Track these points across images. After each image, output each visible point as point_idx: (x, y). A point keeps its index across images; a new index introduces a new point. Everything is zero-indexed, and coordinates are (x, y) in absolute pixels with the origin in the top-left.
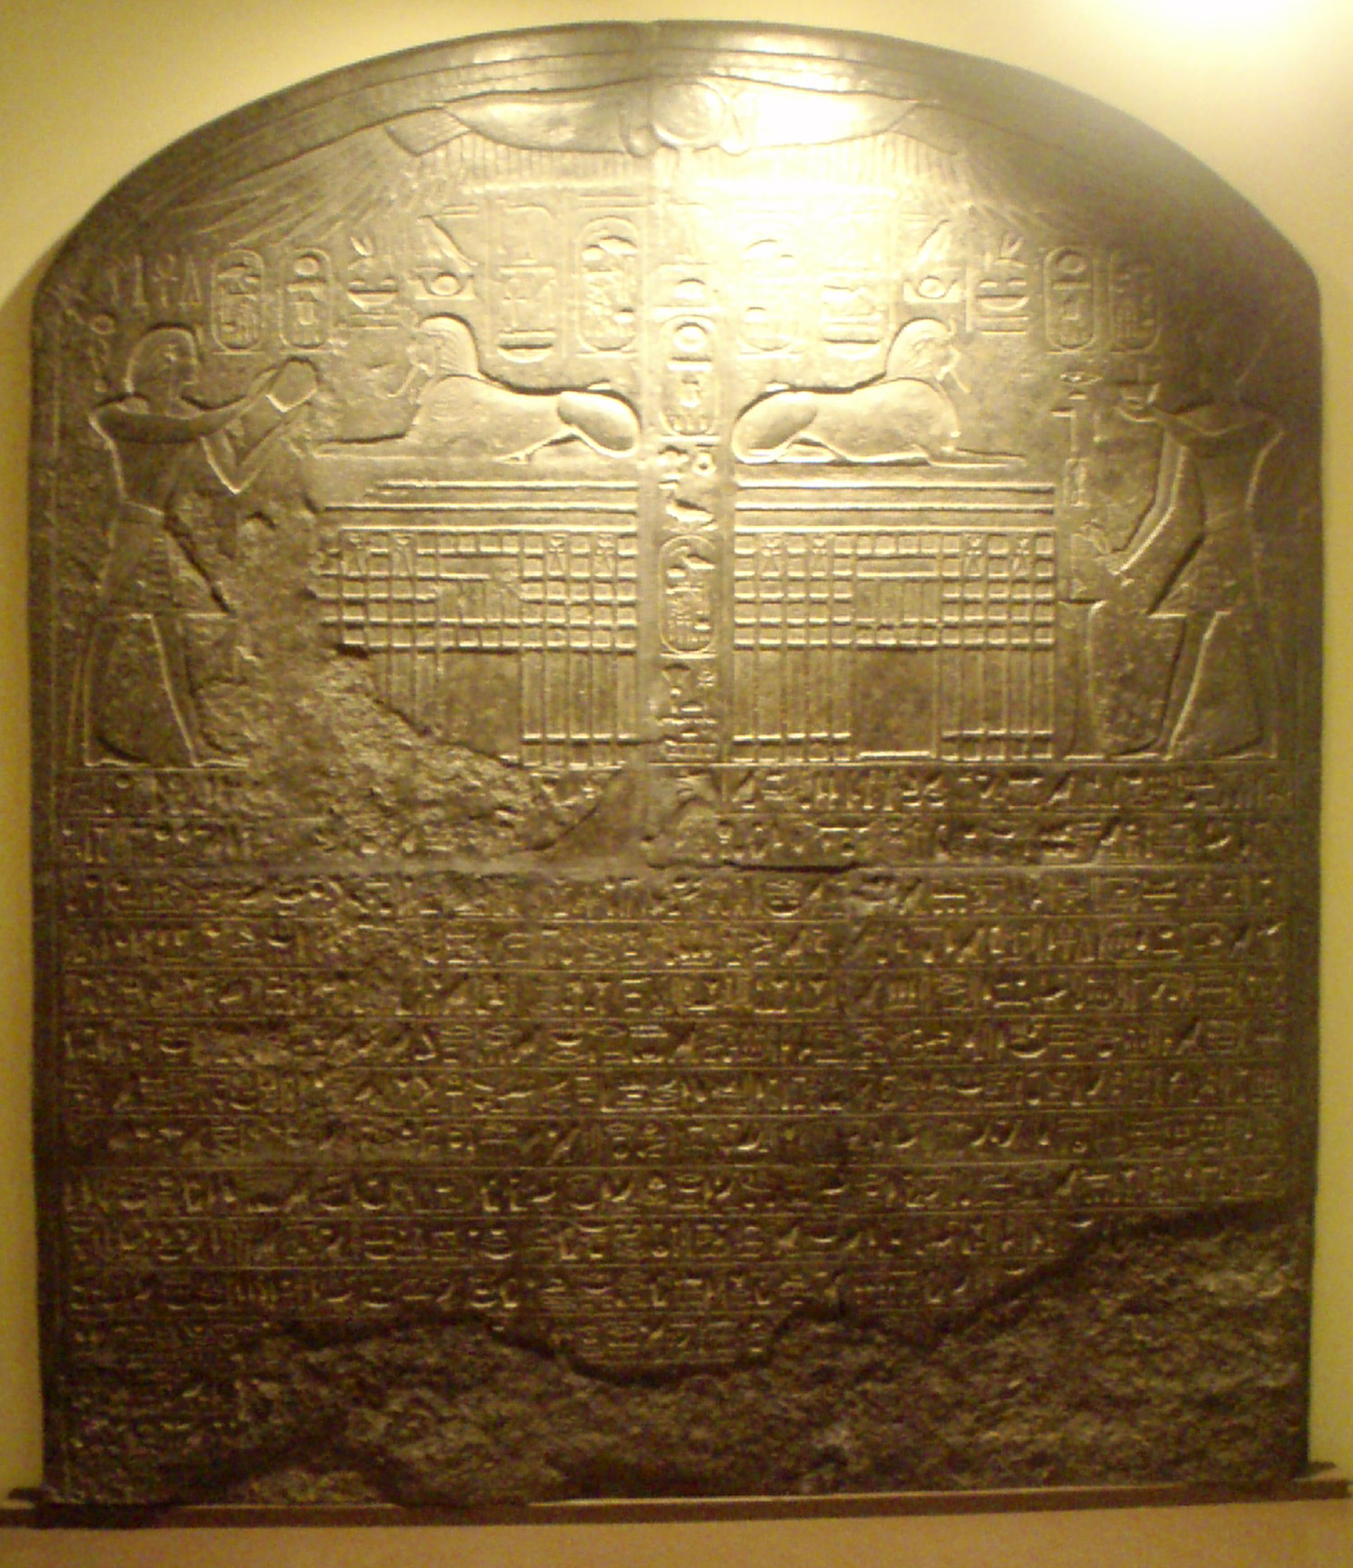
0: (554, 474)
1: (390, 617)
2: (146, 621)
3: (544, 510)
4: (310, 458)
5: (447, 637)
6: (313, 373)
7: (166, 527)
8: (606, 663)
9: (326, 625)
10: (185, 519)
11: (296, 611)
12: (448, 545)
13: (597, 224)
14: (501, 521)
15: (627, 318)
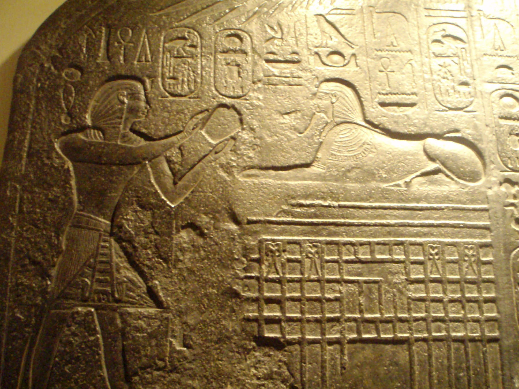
0: (427, 198)
1: (302, 312)
2: (90, 313)
3: (422, 226)
4: (235, 181)
5: (350, 330)
6: (237, 116)
7: (112, 234)
8: (477, 348)
9: (248, 320)
10: (128, 227)
11: (222, 308)
12: (349, 253)
13: (436, 28)
14: (389, 234)
15: (463, 89)
